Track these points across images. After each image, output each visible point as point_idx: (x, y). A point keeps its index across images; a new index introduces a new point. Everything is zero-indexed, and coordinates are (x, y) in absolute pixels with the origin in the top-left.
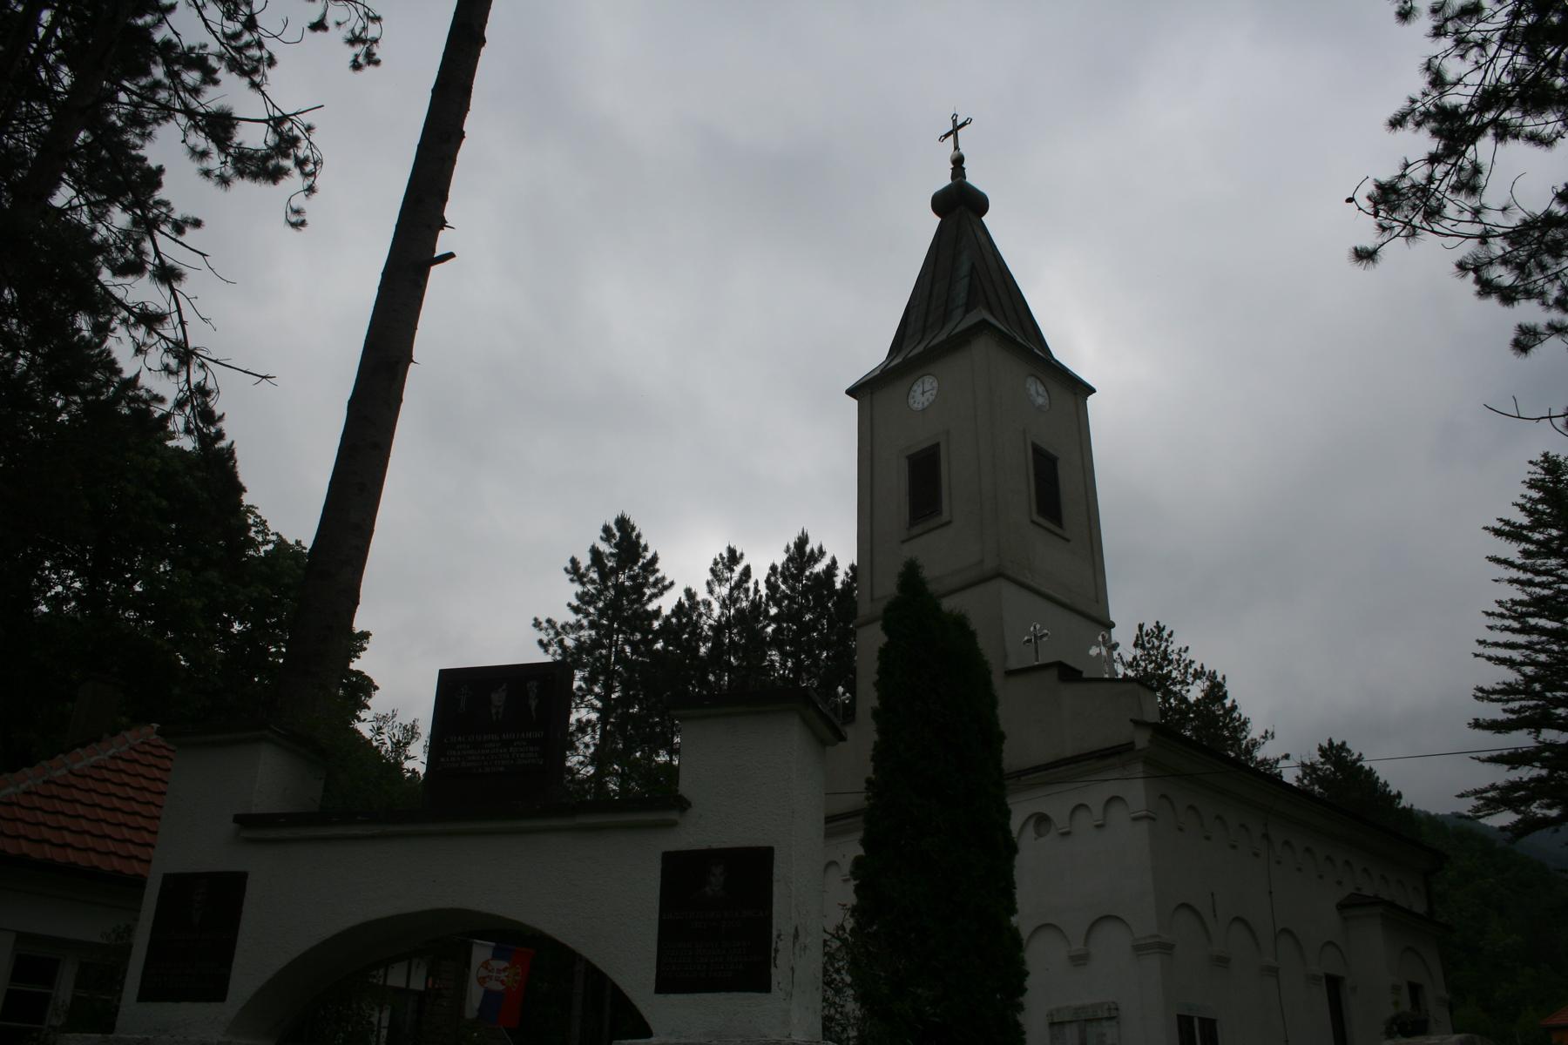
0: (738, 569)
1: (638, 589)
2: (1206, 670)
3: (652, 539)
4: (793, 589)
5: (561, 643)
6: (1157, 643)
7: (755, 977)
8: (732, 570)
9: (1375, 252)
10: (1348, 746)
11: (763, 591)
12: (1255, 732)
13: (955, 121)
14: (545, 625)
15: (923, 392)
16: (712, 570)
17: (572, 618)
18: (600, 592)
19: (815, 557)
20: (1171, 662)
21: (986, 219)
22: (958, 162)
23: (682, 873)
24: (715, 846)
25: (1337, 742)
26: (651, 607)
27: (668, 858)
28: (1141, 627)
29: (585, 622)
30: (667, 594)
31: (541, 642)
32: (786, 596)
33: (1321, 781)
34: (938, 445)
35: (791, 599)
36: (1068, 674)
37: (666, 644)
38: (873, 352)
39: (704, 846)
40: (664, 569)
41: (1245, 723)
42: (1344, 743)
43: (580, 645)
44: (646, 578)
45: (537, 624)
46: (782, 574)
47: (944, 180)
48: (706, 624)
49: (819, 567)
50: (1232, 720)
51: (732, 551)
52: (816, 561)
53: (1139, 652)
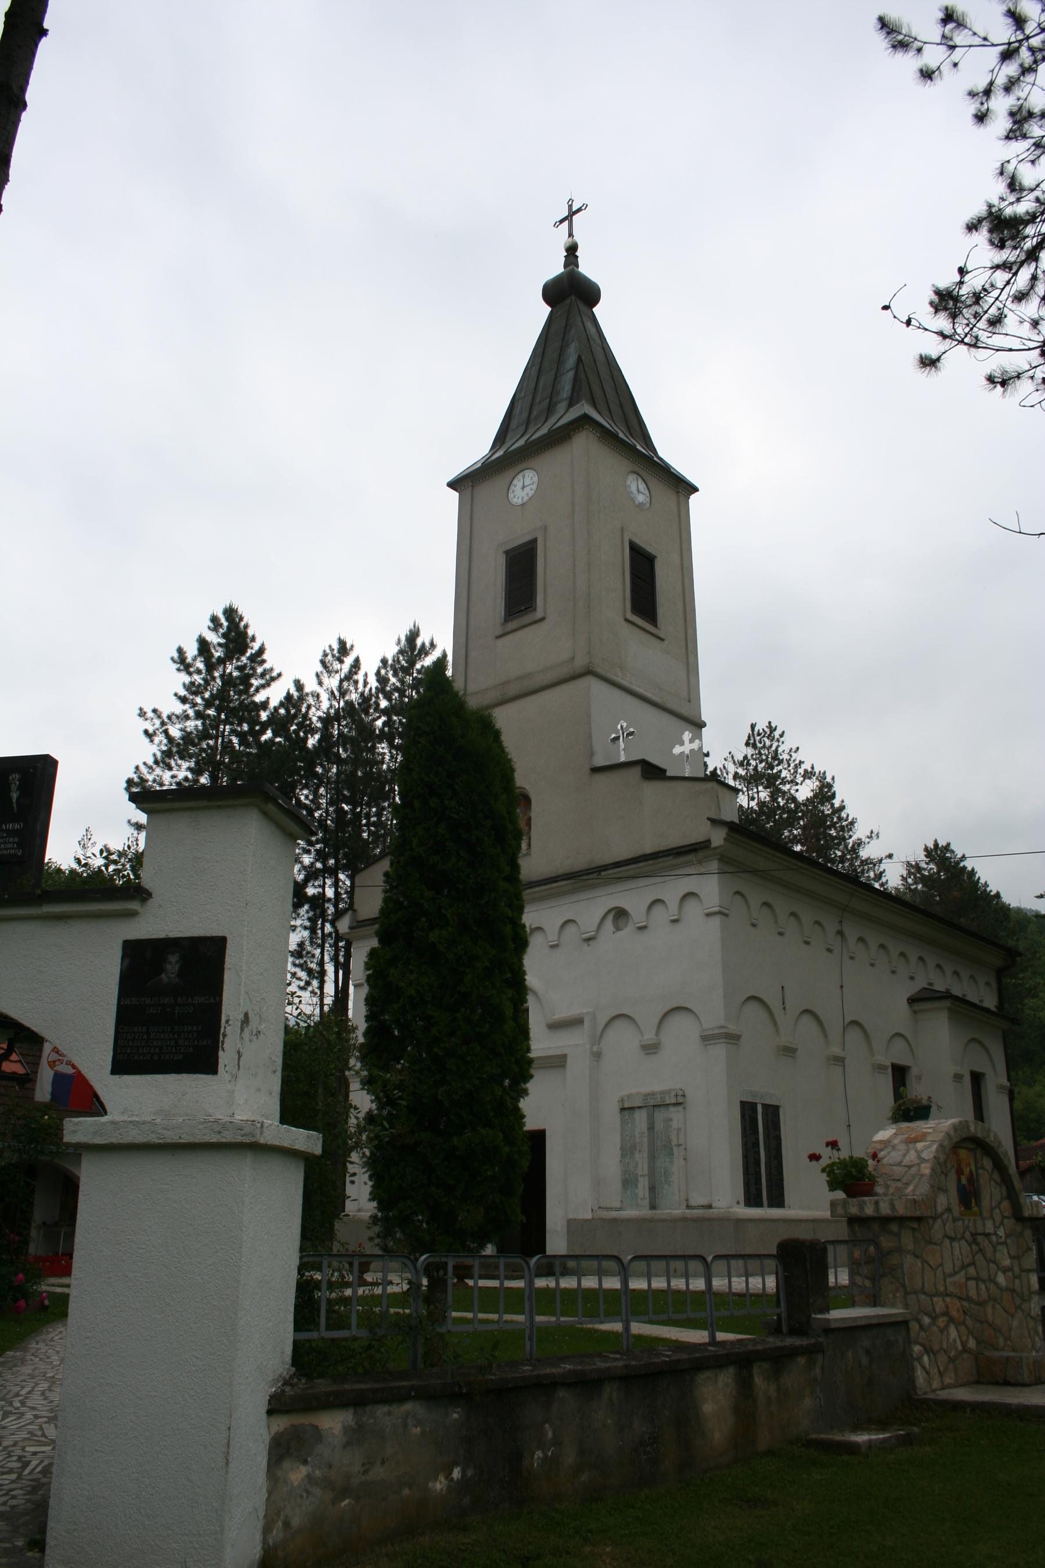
0: (349, 661)
1: (245, 680)
2: (816, 770)
3: (260, 628)
4: (402, 682)
5: (166, 732)
6: (768, 743)
7: (203, 1059)
8: (341, 662)
9: (938, 359)
10: (952, 847)
11: (373, 683)
12: (860, 832)
13: (570, 207)
14: (150, 714)
15: (524, 486)
16: (323, 663)
17: (179, 708)
18: (207, 682)
19: (424, 651)
20: (781, 762)
21: (599, 311)
22: (572, 250)
23: (142, 960)
24: (172, 935)
25: (942, 843)
26: (259, 698)
27: (133, 949)
28: (753, 726)
29: (191, 713)
30: (274, 685)
31: (146, 732)
32: (397, 689)
33: (924, 880)
34: (534, 541)
35: (402, 692)
36: (651, 772)
37: (276, 734)
38: (476, 446)
39: (162, 935)
40: (272, 660)
41: (852, 823)
42: (949, 844)
43: (187, 737)
44: (253, 669)
45: (142, 714)
46: (393, 667)
47: (556, 268)
48: (315, 715)
49: (428, 661)
50: (840, 819)
51: (342, 643)
52: (427, 654)
53: (750, 751)
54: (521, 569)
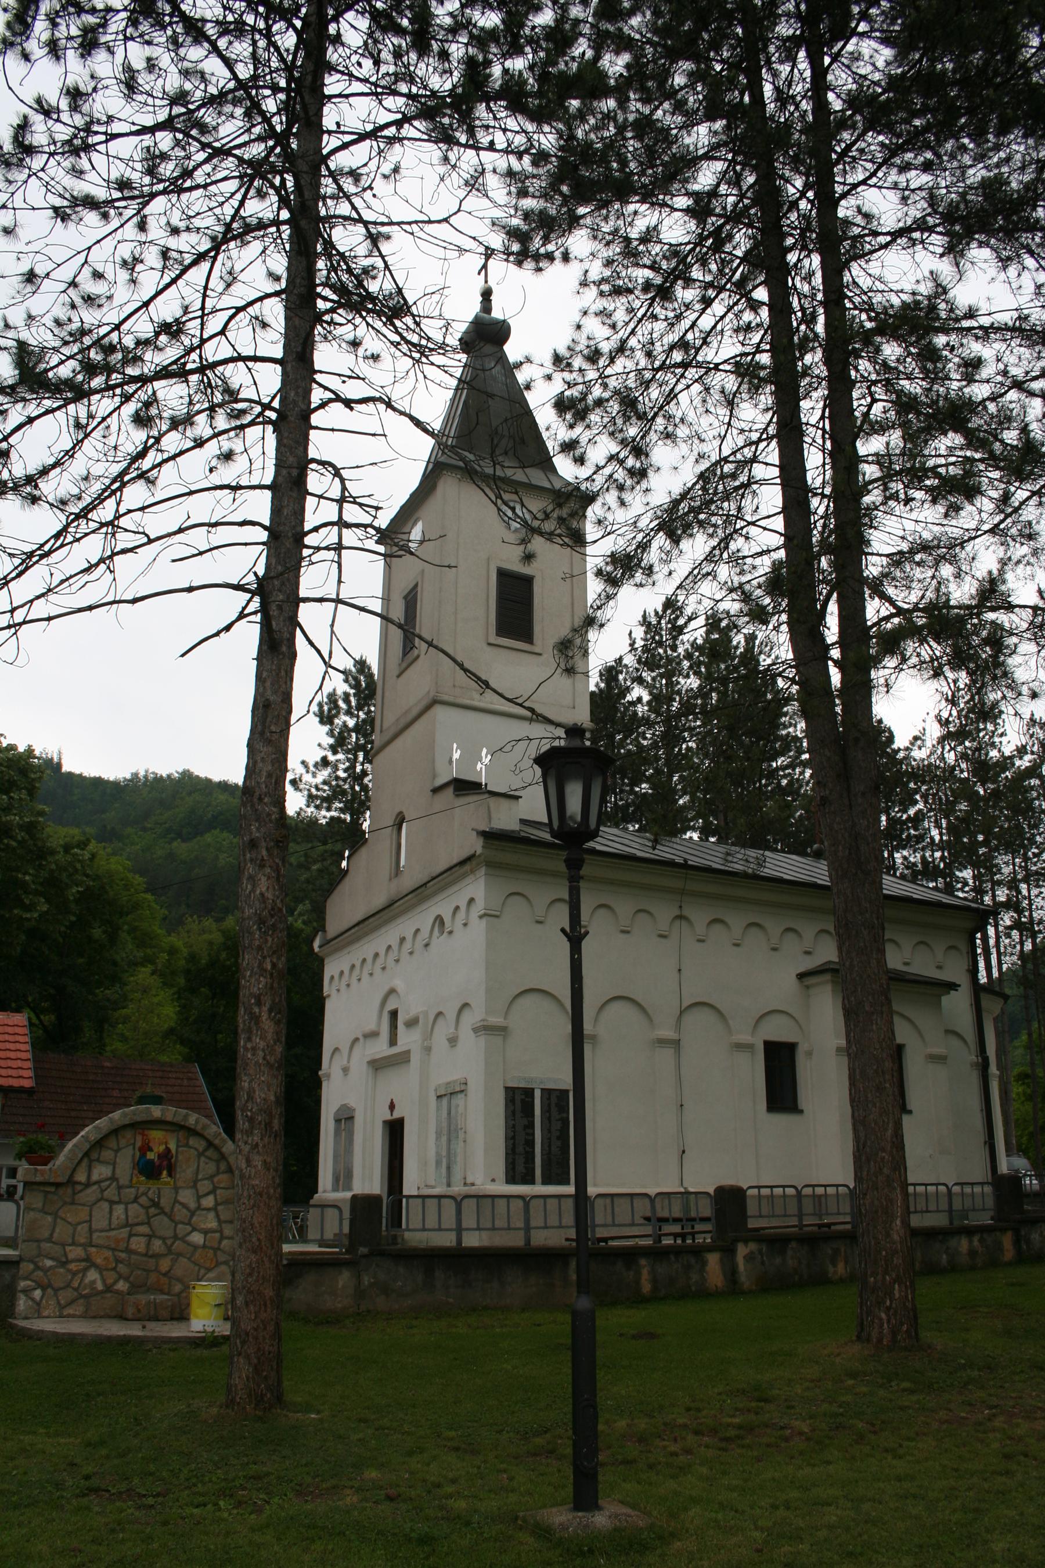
22: (487, 295)
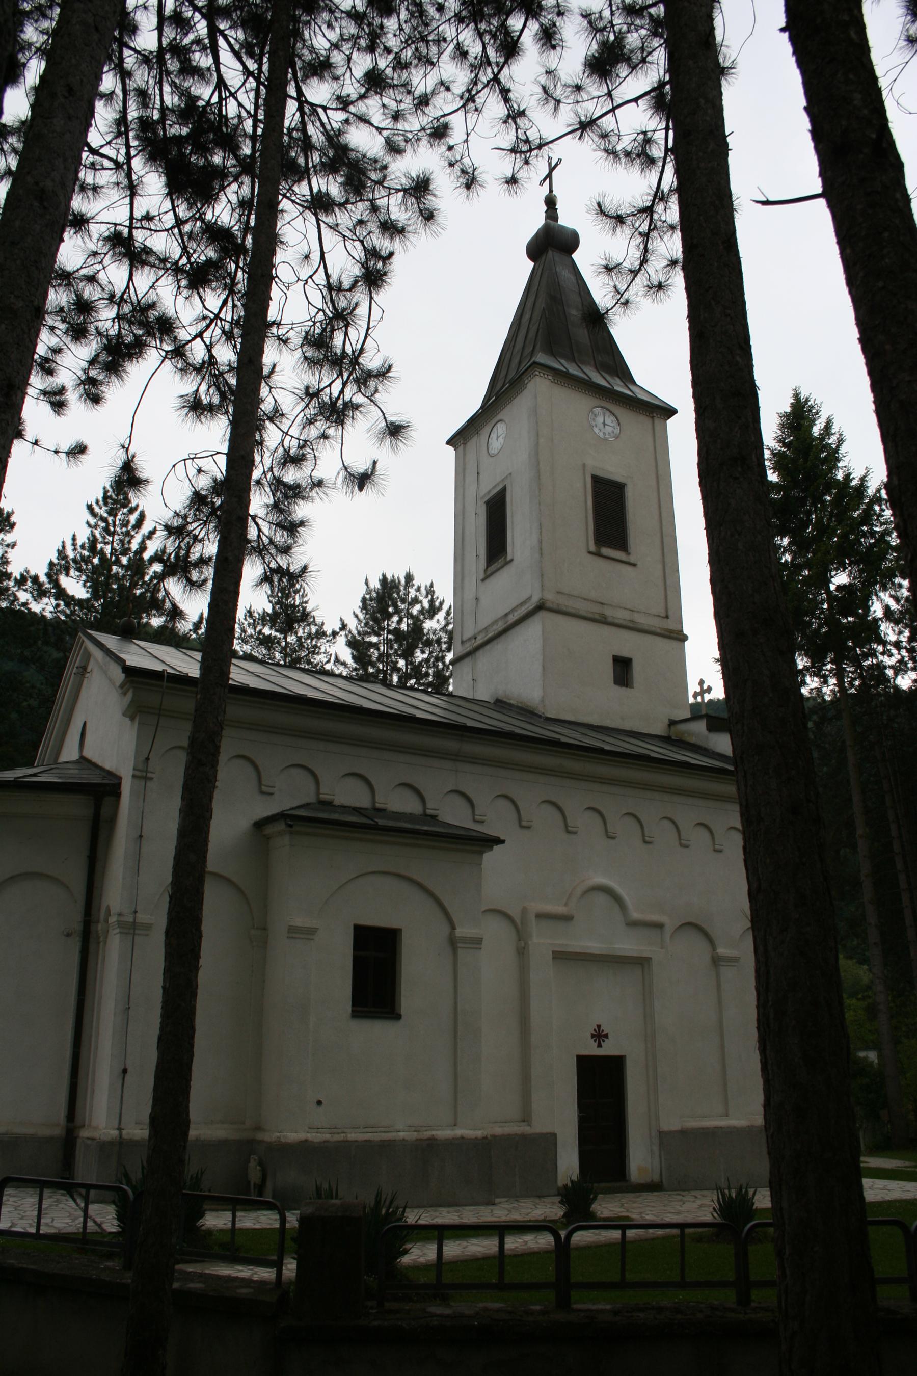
15: (498, 437)
22: (551, 202)
54: (496, 510)
